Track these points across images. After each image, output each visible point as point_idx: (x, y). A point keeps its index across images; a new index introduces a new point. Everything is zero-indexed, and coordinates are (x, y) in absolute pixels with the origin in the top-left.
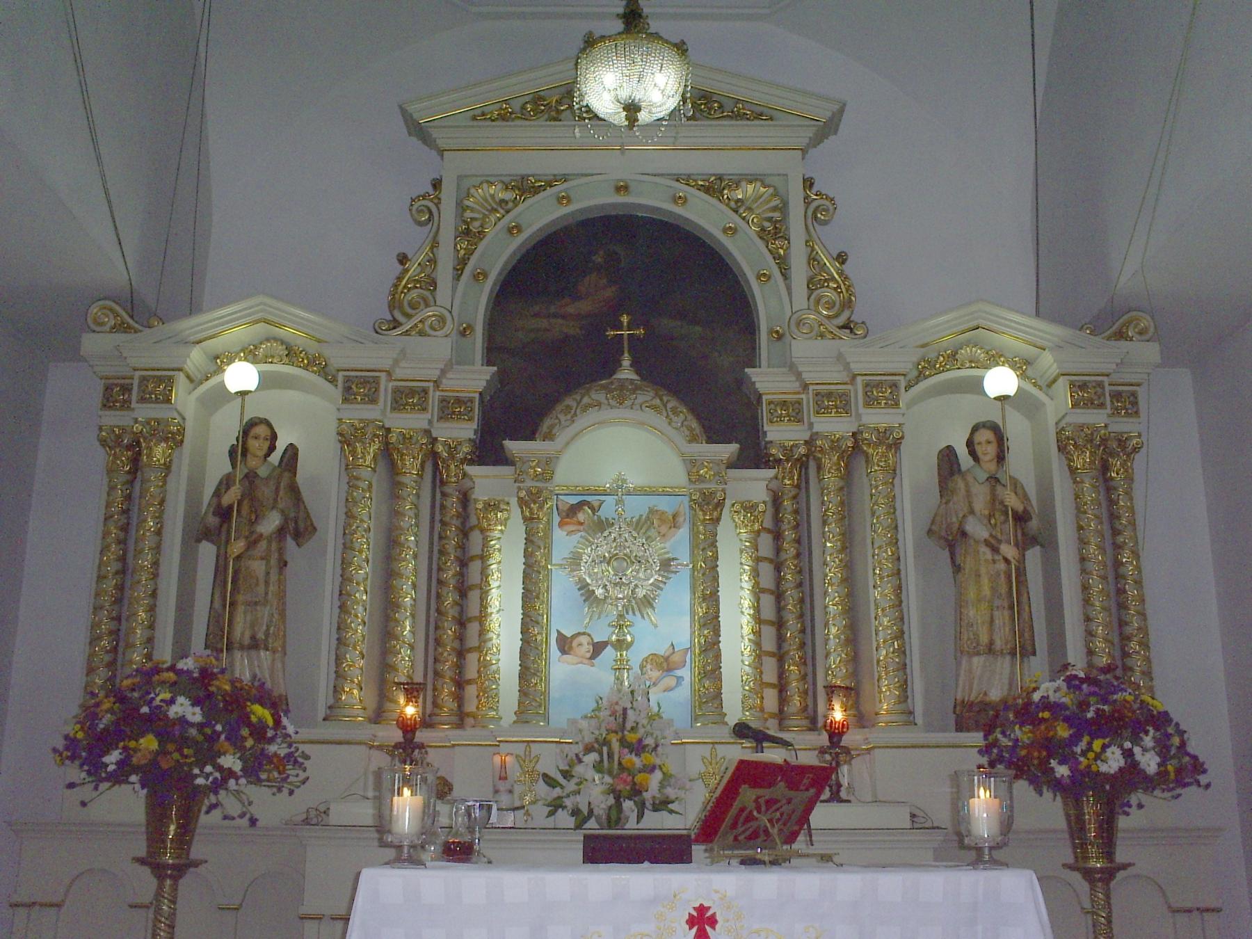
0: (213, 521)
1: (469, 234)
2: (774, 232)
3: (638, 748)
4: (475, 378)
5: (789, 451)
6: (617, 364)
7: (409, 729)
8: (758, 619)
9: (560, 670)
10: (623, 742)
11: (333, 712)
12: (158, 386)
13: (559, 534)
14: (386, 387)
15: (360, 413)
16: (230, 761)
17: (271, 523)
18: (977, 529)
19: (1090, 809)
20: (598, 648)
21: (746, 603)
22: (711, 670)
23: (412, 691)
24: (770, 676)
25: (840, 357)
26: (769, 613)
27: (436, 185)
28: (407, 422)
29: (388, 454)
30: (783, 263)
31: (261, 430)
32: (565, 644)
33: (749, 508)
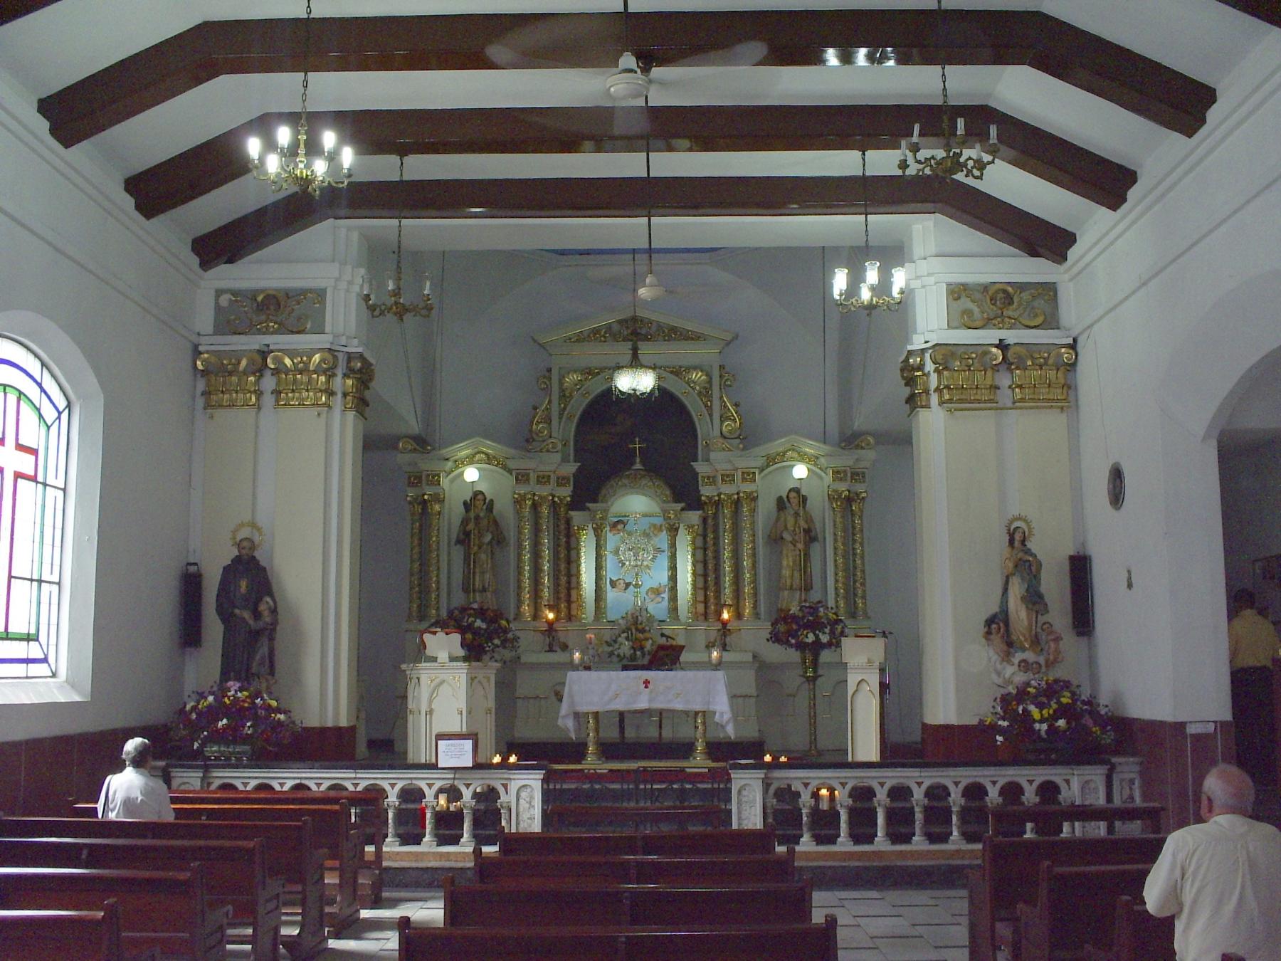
0: (462, 537)
1: (564, 396)
2: (706, 393)
3: (643, 631)
4: (571, 469)
5: (710, 498)
6: (633, 464)
7: (550, 624)
8: (694, 574)
9: (611, 594)
10: (637, 629)
11: (518, 616)
12: (434, 479)
13: (610, 535)
14: (533, 477)
15: (522, 490)
16: (497, 642)
17: (488, 537)
18: (787, 536)
19: (809, 658)
20: (628, 585)
21: (690, 568)
22: (674, 598)
23: (551, 608)
24: (701, 598)
25: (730, 461)
26: (700, 571)
27: (549, 370)
28: (544, 491)
29: (535, 507)
30: (710, 409)
31: (480, 497)
32: (613, 584)
33: (690, 527)
